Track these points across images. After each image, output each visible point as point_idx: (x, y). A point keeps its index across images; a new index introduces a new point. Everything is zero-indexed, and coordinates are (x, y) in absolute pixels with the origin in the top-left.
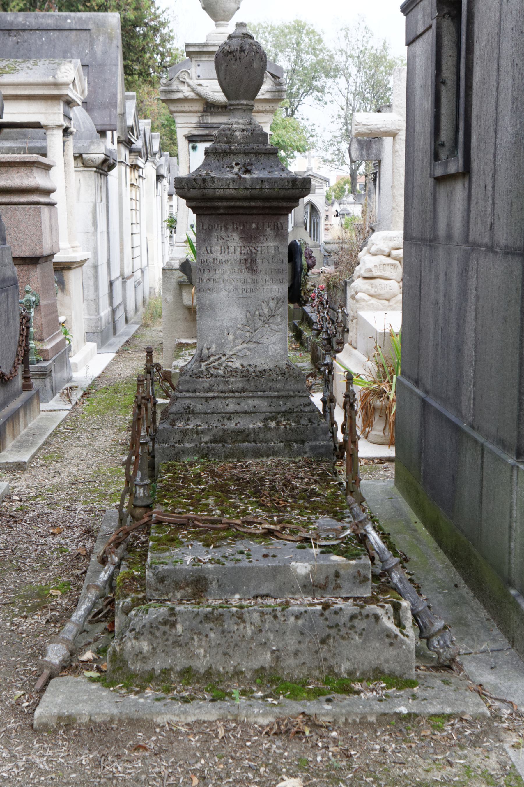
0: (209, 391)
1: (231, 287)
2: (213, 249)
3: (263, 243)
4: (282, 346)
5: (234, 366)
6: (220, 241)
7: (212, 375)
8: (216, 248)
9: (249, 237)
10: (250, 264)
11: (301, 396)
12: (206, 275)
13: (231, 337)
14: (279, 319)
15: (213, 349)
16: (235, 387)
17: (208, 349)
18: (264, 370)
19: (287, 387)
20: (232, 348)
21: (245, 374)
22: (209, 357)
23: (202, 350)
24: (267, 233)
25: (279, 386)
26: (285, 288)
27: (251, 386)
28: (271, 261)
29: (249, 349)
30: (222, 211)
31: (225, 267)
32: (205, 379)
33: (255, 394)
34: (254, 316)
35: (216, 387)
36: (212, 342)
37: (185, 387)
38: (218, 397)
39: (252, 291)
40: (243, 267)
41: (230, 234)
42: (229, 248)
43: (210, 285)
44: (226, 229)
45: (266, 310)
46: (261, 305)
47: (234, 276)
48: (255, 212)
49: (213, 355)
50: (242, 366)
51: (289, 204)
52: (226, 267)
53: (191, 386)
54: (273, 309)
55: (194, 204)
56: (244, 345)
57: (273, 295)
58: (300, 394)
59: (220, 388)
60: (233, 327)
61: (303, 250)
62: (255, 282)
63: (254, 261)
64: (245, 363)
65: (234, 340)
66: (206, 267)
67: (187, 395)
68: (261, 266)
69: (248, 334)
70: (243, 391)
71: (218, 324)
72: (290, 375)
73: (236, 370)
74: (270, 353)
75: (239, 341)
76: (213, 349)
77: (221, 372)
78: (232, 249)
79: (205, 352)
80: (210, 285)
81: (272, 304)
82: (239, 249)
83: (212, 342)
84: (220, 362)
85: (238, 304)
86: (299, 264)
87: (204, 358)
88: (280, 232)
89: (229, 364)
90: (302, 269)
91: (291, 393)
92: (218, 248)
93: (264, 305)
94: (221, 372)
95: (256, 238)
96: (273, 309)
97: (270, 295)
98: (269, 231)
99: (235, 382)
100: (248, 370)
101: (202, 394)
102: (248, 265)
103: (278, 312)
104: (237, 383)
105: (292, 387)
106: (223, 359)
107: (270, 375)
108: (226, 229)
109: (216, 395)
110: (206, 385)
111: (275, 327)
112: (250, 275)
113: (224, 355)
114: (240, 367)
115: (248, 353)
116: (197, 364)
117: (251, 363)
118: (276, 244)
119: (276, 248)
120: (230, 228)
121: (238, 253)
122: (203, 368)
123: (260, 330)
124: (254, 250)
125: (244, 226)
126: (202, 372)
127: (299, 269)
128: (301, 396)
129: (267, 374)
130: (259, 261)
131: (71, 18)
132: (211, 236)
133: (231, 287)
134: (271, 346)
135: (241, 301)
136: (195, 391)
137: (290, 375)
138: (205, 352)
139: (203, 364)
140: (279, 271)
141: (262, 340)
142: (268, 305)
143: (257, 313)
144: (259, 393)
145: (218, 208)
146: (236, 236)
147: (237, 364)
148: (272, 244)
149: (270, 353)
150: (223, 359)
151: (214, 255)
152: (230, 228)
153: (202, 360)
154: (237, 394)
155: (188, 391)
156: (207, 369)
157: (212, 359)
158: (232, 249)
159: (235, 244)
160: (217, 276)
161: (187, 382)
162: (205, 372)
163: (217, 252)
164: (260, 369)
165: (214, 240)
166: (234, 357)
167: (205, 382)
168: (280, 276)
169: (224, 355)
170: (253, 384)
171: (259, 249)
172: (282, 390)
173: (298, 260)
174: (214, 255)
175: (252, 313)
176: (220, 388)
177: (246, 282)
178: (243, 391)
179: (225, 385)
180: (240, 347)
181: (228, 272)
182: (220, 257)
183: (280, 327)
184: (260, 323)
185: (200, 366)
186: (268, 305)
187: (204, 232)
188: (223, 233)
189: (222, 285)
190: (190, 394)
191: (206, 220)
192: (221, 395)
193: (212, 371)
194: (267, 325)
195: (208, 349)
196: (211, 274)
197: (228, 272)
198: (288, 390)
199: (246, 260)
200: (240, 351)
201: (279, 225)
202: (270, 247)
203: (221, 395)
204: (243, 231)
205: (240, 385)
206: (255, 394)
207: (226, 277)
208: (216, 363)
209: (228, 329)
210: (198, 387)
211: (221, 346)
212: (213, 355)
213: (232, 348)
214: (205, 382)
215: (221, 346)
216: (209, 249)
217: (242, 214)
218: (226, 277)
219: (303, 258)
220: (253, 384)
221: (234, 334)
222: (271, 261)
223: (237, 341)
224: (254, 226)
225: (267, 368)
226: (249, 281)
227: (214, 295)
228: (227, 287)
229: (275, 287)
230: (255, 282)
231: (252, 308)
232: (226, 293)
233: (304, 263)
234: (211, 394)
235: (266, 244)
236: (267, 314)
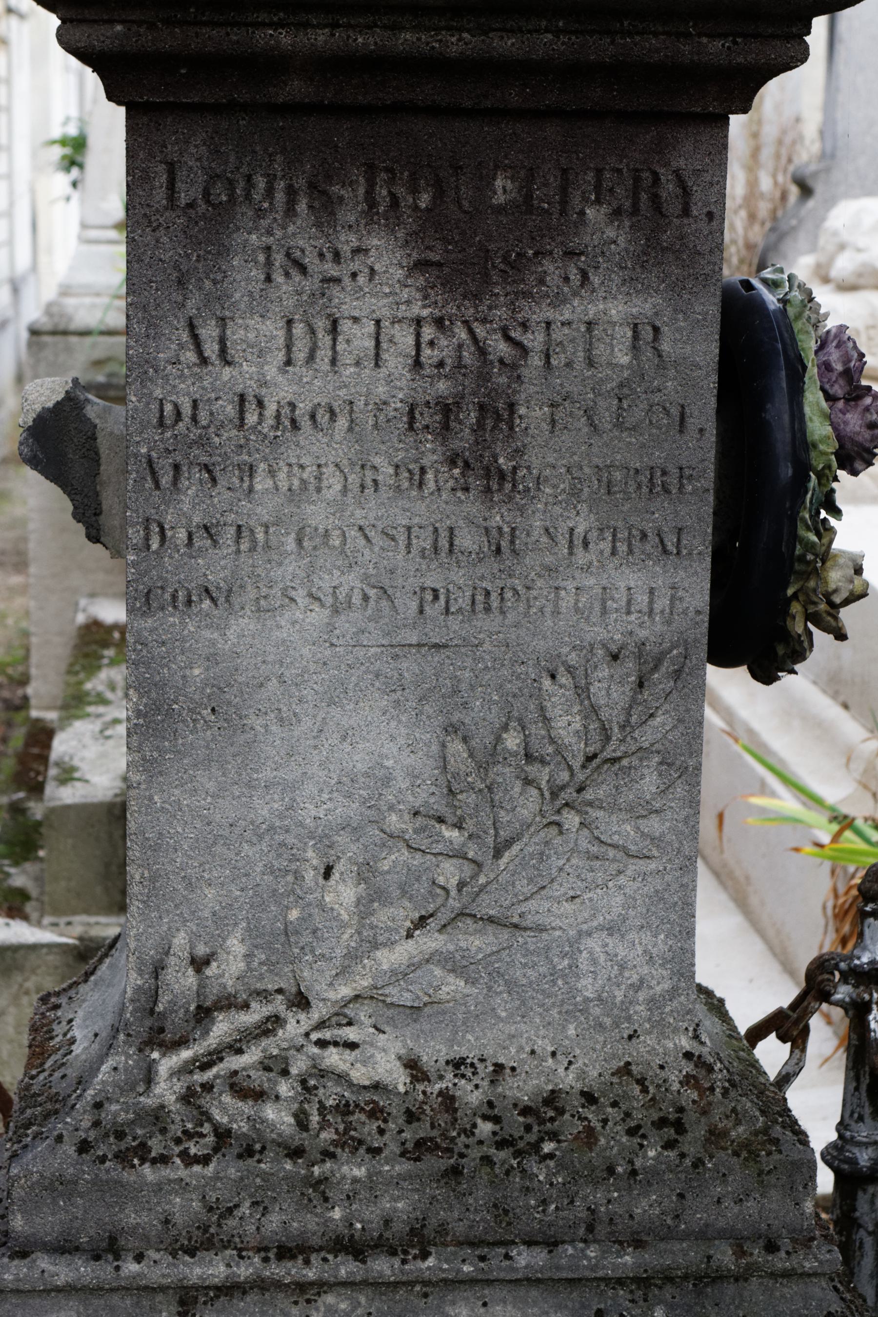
0: (200, 1242)
1: (352, 580)
2: (235, 334)
3: (559, 301)
4: (661, 944)
5: (360, 1075)
6: (284, 286)
7: (223, 1135)
8: (258, 331)
9: (471, 262)
10: (471, 431)
11: (788, 1275)
12: (189, 505)
13: (344, 894)
14: (649, 782)
15: (230, 968)
16: (368, 1216)
17: (199, 964)
18: (552, 1099)
19: (699, 1215)
20: (353, 956)
21: (432, 1128)
22: (204, 1014)
23: (158, 969)
24: (588, 239)
25: (647, 1206)
26: (694, 587)
27: (471, 1211)
28: (605, 419)
29: (456, 965)
30: (295, 89)
31: (311, 448)
32: (178, 1170)
33: (496, 1265)
34: (489, 758)
35: (245, 1222)
36: (222, 921)
37: (48, 1222)
38: (261, 1285)
39: (483, 602)
40: (431, 452)
41: (347, 241)
42: (341, 330)
43: (215, 565)
44: (326, 209)
45: (568, 725)
46: (537, 694)
47: (370, 511)
48: (514, 97)
49: (229, 1003)
50: (412, 1066)
51: (747, 54)
52: (319, 450)
53: (87, 1218)
54: (613, 715)
55: (111, 34)
56: (430, 941)
57: (614, 630)
58: (780, 1261)
59: (274, 1222)
60: (356, 831)
61: (809, 345)
62: (501, 547)
63: (497, 415)
64: (434, 1052)
65: (364, 908)
66: (193, 449)
67: (62, 1271)
68: (546, 446)
69: (449, 873)
70: (419, 1239)
71: (264, 809)
72: (715, 1136)
73: (373, 1101)
74: (588, 987)
75: (402, 914)
76: (230, 968)
77: (278, 1117)
78: (358, 338)
79: (181, 982)
80: (215, 565)
81: (610, 690)
82: (405, 339)
83: (222, 921)
84: (272, 1045)
85: (395, 687)
86: (782, 437)
87: (176, 1023)
88: (672, 220)
89: (334, 1058)
90: (802, 469)
91: (725, 1256)
92: (274, 329)
93: (558, 696)
94: (278, 1117)
95: (516, 266)
96: (613, 715)
97: (596, 633)
98: (601, 226)
99: (372, 1186)
100: (448, 1099)
101: (159, 1269)
102: (463, 440)
103: (647, 736)
104: (375, 1189)
105: (731, 1214)
106: (295, 1026)
107: (589, 1136)
108: (326, 209)
109: (244, 1272)
110: (184, 1208)
111: (622, 830)
112: (472, 505)
113: (301, 1002)
114: (400, 1079)
115: (453, 986)
116: (123, 1059)
117: (467, 1049)
118: (643, 306)
119: (645, 335)
120: (351, 197)
121: (396, 362)
122: (166, 1091)
123: (528, 845)
124: (500, 348)
125: (439, 195)
126: (158, 1117)
127: (787, 471)
128: (788, 1275)
129: (571, 1127)
130: (532, 415)
131: (864, 1087)
132: (224, 252)
133: (352, 580)
134: (593, 944)
135: (409, 666)
136: (110, 1248)
137: (715, 1136)
138: (181, 982)
139: (167, 1064)
140: (657, 483)
141: (537, 909)
142: (582, 691)
143: (512, 741)
144: (525, 1258)
145: (276, 65)
146: (387, 256)
147: (381, 1062)
148: (615, 308)
149: (588, 987)
150: (295, 1026)
151: (244, 375)
152: (351, 197)
153: (159, 1036)
154: (383, 1266)
155: (64, 1248)
156: (188, 1097)
157: (222, 1028)
158: (358, 338)
159: (382, 307)
160: (264, 513)
161: (59, 1186)
162: (180, 1119)
163: (259, 353)
164: (522, 1088)
165: (244, 276)
166: (362, 1013)
167: (177, 1190)
168: (661, 515)
169: (301, 1002)
170: (481, 1195)
171: (535, 340)
172: (669, 1235)
173: (778, 411)
174: (244, 375)
175: (482, 739)
176: (274, 1222)
177: (443, 546)
178: (419, 1239)
179: (305, 1205)
180: (400, 954)
181: (334, 483)
182: (281, 390)
183: (654, 825)
184: (528, 805)
185: (149, 1079)
186: (582, 691)
187: (175, 227)
188: (302, 236)
189: (291, 568)
190: (82, 1270)
191: (193, 154)
192: (276, 1270)
193: (226, 1110)
194: (571, 820)
195: (199, 964)
196: (221, 496)
197: (334, 483)
198: (704, 1235)
199: (447, 410)
200: (399, 975)
201: (668, 188)
202: (604, 327)
203: (276, 1270)
204: (431, 224)
205: (400, 1206)
206: (496, 1265)
207: (317, 514)
208: (251, 1056)
209: (324, 841)
210: (131, 1218)
211: (280, 942)
212: (229, 1003)
213: (353, 956)
214: (177, 1190)
215: (280, 942)
216: (209, 332)
217: (434, 111)
218: (317, 514)
219: (813, 399)
220: (481, 1195)
221: (365, 872)
222: (605, 419)
223: (383, 916)
224: (503, 189)
225: (568, 1080)
226: (467, 540)
227: (243, 625)
228: (325, 582)
229: (630, 580)
230: (501, 547)
231: (482, 714)
232: (319, 616)
233: (819, 429)
234: (214, 1269)
235: (578, 309)
236: (578, 749)
